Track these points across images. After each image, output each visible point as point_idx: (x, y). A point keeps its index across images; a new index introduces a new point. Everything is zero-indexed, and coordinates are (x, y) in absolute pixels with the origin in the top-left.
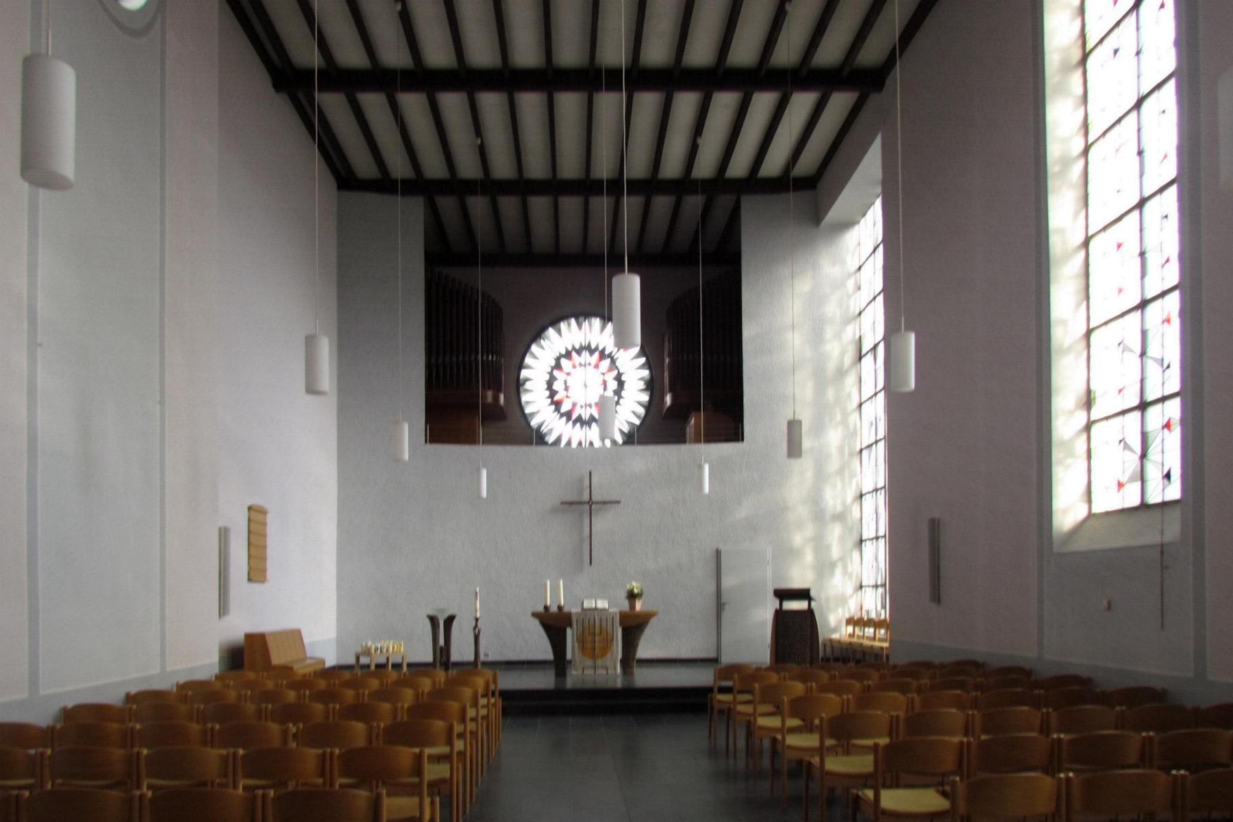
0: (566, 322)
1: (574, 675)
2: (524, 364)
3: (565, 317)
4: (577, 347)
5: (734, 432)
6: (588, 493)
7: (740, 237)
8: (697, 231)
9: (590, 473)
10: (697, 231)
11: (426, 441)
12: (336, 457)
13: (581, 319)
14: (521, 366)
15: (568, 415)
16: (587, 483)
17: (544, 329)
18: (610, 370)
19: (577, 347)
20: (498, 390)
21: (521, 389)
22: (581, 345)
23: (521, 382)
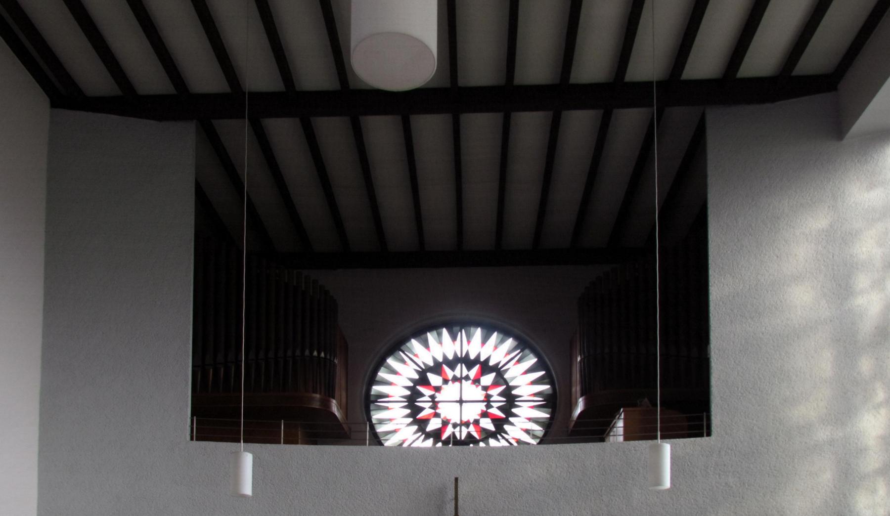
0: (435, 333)
1: (579, 398)
2: (377, 379)
3: (435, 327)
4: (450, 357)
5: (709, 434)
6: (453, 508)
7: (705, 177)
8: (651, 126)
9: (456, 479)
10: (651, 126)
11: (192, 439)
12: (36, 449)
13: (456, 329)
14: (373, 380)
15: (436, 435)
16: (451, 494)
17: (407, 339)
18: (495, 384)
19: (450, 357)
20: (330, 393)
21: (372, 407)
22: (455, 354)
23: (372, 399)
